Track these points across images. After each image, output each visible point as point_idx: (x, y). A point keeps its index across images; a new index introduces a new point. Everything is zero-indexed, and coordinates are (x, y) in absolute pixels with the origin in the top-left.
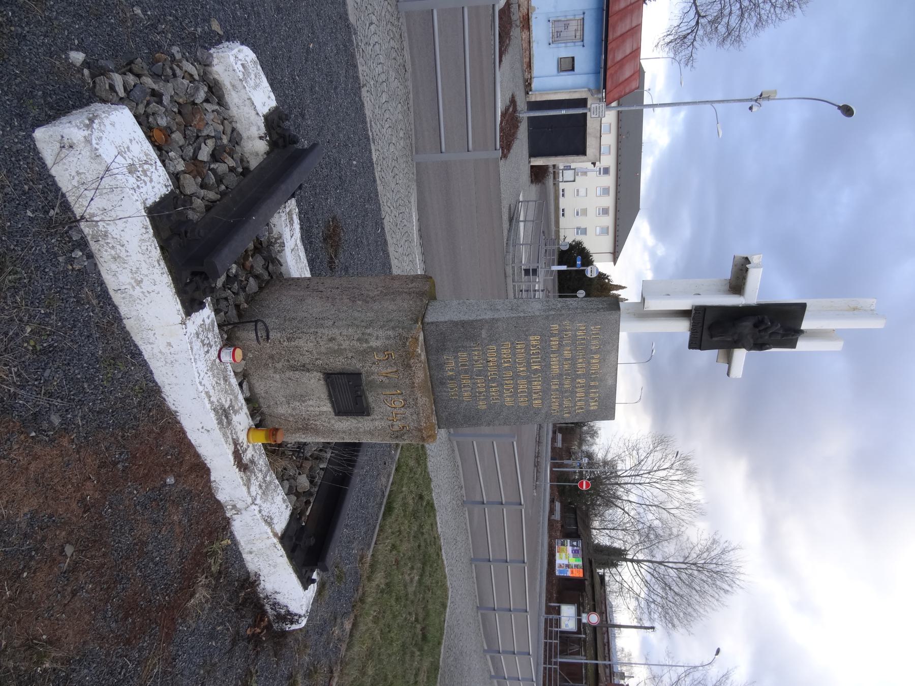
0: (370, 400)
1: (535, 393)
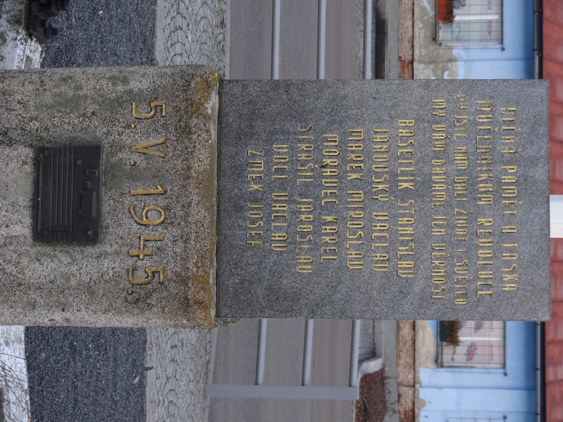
0: (106, 208)
1: (403, 243)
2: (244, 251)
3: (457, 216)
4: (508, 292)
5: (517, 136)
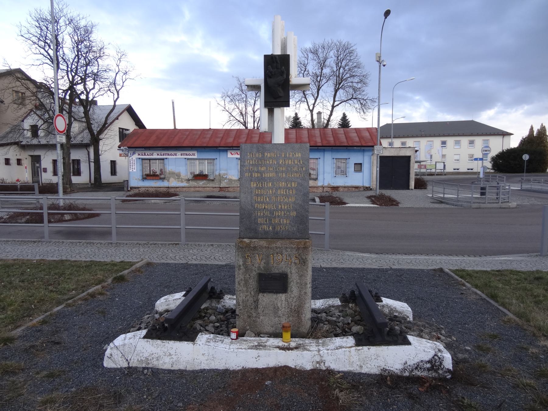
0: (277, 272)
1: (287, 185)
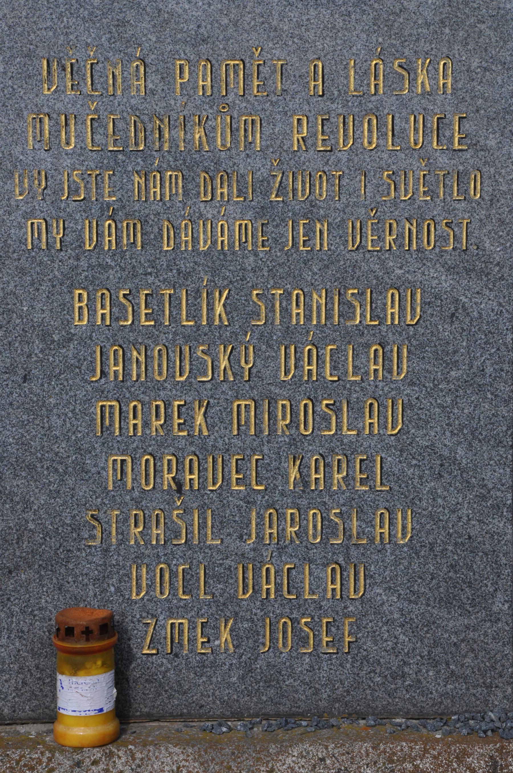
2: (366, 658)
3: (286, 195)
4: (455, 81)
5: (107, 59)
